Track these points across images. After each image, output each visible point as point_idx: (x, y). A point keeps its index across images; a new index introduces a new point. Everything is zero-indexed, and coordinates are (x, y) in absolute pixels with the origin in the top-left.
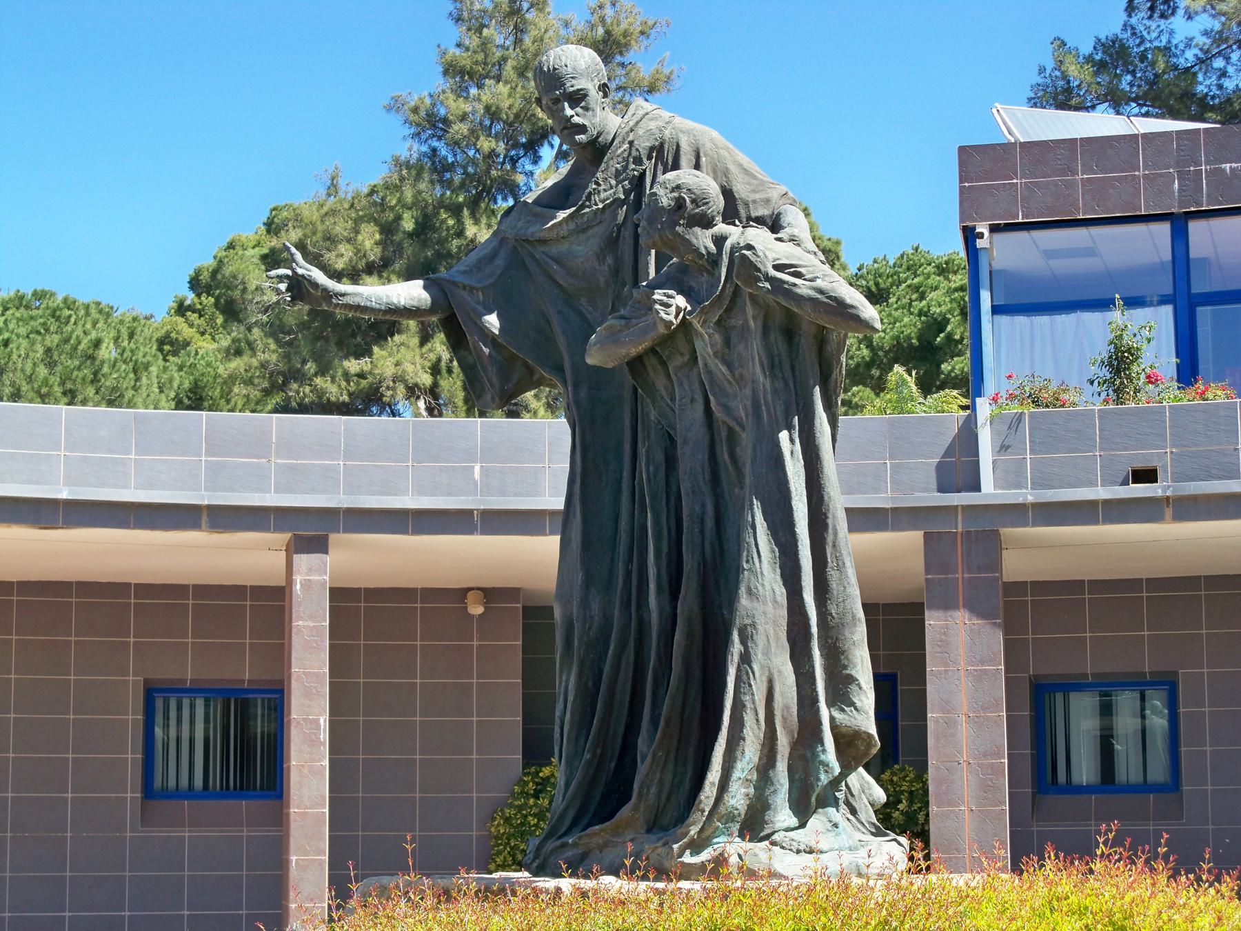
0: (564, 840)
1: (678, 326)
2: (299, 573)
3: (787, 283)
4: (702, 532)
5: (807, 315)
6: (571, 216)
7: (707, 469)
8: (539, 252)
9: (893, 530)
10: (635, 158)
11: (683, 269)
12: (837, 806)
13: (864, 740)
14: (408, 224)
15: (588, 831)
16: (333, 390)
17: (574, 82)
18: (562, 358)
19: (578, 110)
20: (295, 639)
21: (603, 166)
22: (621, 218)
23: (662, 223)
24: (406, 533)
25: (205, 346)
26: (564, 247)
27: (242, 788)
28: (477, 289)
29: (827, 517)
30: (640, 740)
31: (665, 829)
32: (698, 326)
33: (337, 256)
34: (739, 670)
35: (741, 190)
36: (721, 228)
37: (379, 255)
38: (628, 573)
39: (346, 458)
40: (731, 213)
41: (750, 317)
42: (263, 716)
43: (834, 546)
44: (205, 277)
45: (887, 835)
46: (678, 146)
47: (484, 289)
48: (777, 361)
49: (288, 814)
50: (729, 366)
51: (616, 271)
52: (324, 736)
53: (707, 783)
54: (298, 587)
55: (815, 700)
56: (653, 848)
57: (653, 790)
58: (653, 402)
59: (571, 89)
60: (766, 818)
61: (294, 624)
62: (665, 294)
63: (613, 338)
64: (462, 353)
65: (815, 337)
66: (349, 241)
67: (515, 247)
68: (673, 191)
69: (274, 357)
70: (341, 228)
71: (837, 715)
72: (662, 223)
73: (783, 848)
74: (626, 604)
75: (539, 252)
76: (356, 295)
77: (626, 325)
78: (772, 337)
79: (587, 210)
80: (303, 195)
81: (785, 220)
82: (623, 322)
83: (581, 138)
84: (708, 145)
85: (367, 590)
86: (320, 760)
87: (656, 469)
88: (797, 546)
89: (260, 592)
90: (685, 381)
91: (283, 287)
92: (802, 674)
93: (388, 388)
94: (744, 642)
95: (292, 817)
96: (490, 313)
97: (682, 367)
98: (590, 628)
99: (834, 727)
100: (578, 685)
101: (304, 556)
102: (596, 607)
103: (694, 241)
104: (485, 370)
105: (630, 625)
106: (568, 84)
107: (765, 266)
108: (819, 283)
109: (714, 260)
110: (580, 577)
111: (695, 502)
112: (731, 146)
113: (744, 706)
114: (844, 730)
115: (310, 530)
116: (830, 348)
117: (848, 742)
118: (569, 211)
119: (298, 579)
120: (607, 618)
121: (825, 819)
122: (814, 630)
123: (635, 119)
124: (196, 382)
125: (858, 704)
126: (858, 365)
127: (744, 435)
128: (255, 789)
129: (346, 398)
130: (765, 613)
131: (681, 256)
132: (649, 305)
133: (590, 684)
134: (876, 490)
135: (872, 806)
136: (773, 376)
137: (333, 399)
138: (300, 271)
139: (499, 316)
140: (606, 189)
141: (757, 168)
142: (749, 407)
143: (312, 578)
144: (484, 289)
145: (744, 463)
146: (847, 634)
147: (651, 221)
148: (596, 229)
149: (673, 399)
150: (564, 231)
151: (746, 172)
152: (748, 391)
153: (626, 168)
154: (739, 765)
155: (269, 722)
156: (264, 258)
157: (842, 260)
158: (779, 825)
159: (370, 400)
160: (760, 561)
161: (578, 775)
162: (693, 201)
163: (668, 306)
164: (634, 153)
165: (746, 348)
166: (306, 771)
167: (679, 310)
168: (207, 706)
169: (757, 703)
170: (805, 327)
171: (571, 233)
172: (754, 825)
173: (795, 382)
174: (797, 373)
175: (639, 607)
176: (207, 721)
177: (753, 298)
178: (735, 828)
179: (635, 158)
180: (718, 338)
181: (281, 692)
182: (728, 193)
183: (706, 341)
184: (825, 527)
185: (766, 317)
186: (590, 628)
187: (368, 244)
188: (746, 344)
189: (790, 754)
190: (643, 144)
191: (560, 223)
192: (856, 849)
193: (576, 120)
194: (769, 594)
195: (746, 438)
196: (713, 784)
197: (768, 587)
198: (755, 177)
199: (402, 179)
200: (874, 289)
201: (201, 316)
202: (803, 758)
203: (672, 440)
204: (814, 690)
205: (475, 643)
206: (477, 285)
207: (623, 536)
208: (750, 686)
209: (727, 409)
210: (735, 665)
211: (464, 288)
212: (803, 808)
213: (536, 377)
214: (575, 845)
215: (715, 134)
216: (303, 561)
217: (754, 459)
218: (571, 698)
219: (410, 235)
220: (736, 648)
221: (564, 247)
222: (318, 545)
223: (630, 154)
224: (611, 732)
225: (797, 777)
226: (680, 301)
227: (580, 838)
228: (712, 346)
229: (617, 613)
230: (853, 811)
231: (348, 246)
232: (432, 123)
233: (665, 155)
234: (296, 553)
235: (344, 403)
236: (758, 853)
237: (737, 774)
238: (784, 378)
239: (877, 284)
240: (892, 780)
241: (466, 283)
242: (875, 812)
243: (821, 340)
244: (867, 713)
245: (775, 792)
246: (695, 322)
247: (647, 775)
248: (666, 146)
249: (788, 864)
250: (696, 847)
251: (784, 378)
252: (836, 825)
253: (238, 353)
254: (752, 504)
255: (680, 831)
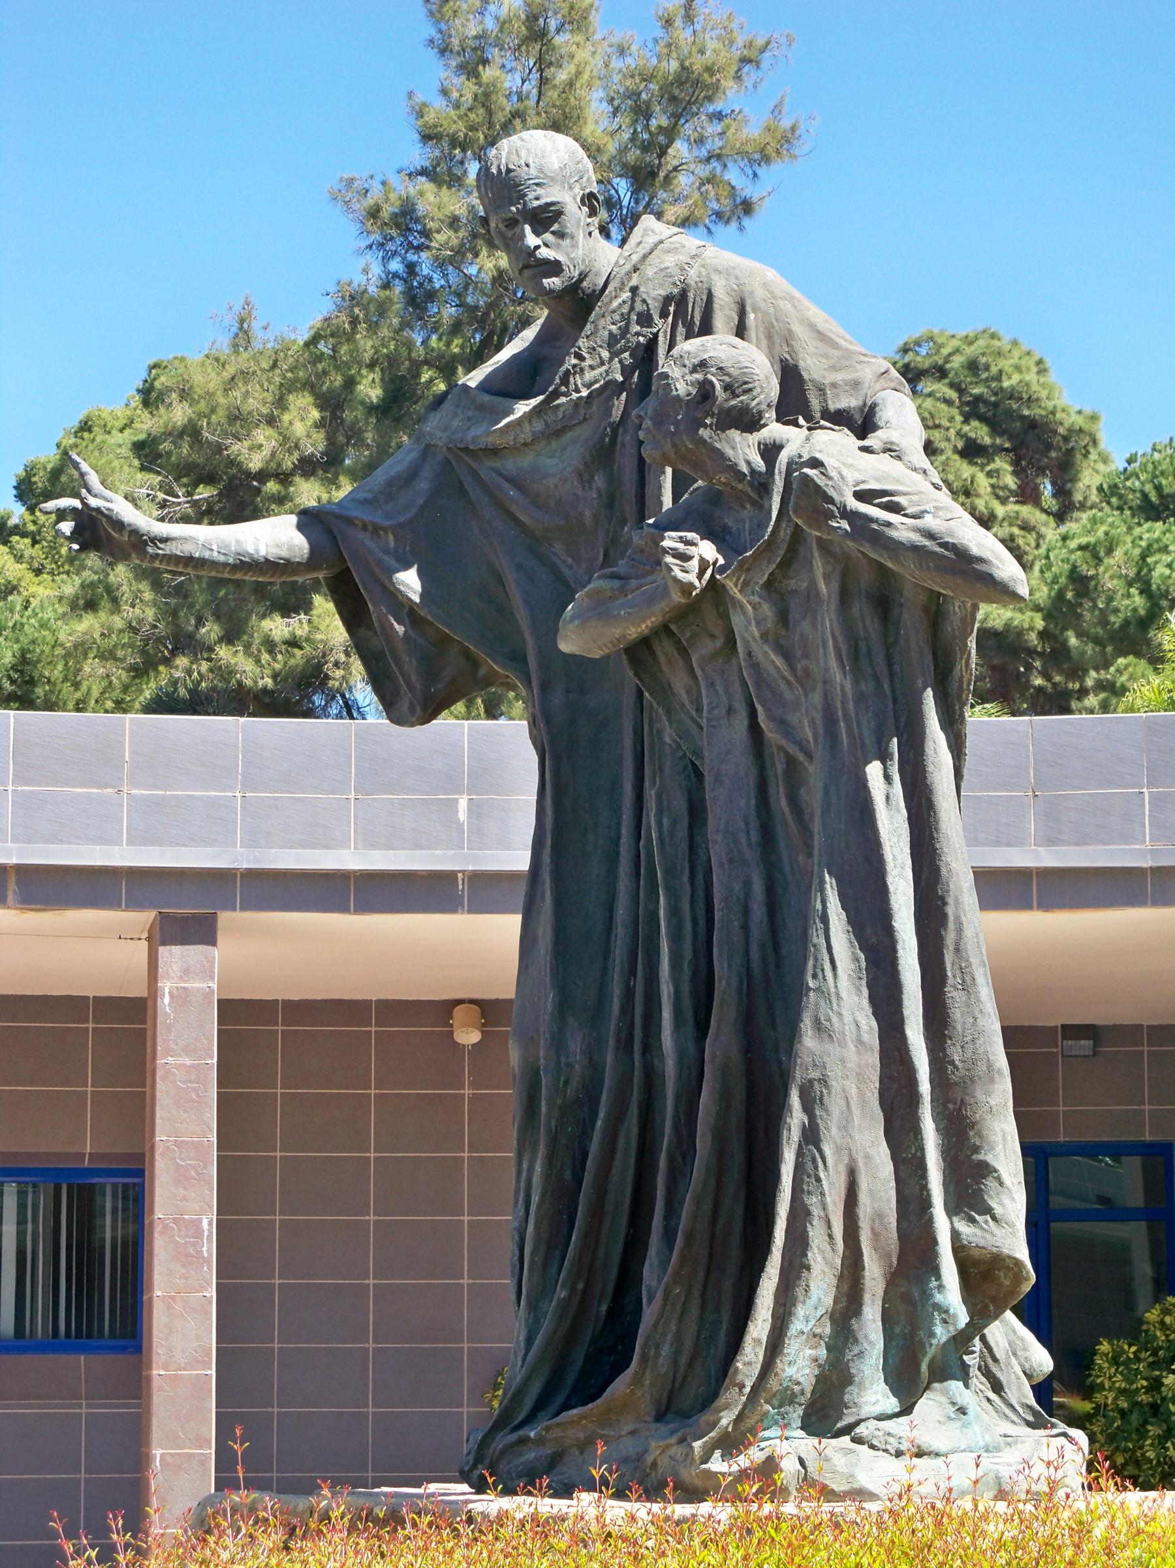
0: (521, 1432)
1: (703, 590)
2: (168, 977)
3: (876, 521)
4: (745, 927)
5: (908, 572)
6: (537, 411)
7: (754, 824)
8: (486, 468)
9: (1155, 903)
10: (639, 315)
11: (714, 498)
12: (965, 1378)
13: (1009, 1269)
14: (370, 389)
15: (559, 1419)
16: (250, 670)
17: (540, 191)
18: (524, 641)
19: (548, 236)
20: (161, 1087)
21: (588, 328)
22: (617, 413)
23: (677, 423)
24: (344, 909)
25: (41, 591)
26: (526, 461)
27: (79, 1335)
28: (385, 530)
29: (945, 904)
30: (646, 1270)
31: (686, 1415)
32: (735, 591)
33: (251, 449)
34: (800, 1154)
35: (812, 366)
36: (774, 430)
37: (321, 447)
38: (629, 994)
39: (245, 787)
40: (795, 400)
41: (820, 577)
42: (114, 1211)
43: (957, 950)
44: (40, 480)
45: (1053, 1426)
46: (710, 295)
47: (397, 529)
48: (863, 647)
49: (149, 1379)
50: (786, 654)
51: (610, 500)
52: (209, 1248)
53: (748, 1340)
54: (167, 1000)
55: (927, 1204)
56: (660, 1448)
57: (666, 1350)
58: (669, 712)
59: (536, 203)
60: (847, 1398)
61: (160, 1062)
62: (681, 540)
63: (601, 608)
64: (362, 632)
65: (926, 609)
66: (271, 421)
67: (447, 461)
68: (694, 370)
69: (150, 614)
70: (256, 401)
71: (963, 1227)
72: (677, 423)
73: (872, 1447)
74: (625, 1045)
75: (486, 468)
76: (186, 539)
77: (622, 587)
78: (855, 610)
79: (563, 400)
80: (194, 342)
81: (885, 414)
82: (616, 584)
83: (553, 282)
84: (760, 293)
85: (286, 1003)
86: (202, 1288)
87: (674, 823)
88: (895, 951)
89: (109, 1007)
90: (718, 680)
91: (67, 527)
92: (905, 1160)
93: (337, 664)
94: (808, 1108)
95: (156, 1383)
96: (406, 566)
97: (714, 655)
98: (567, 1082)
99: (959, 1249)
100: (546, 1177)
101: (176, 949)
102: (576, 1046)
103: (729, 452)
104: (398, 664)
105: (631, 1079)
106: (531, 196)
107: (841, 494)
108: (929, 522)
109: (762, 484)
110: (548, 1000)
111: (732, 877)
112: (797, 294)
113: (808, 1214)
114: (976, 1253)
115: (187, 906)
116: (951, 626)
117: (982, 1275)
118: (541, 398)
119: (166, 986)
120: (594, 1066)
121: (944, 1400)
122: (925, 1087)
123: (642, 251)
124: (23, 652)
125: (998, 1210)
126: (1126, 623)
127: (811, 769)
128: (101, 1334)
129: (269, 682)
130: (843, 1061)
131: (708, 478)
132: (654, 559)
133: (568, 1174)
134: (1127, 838)
135: (1029, 1377)
136: (857, 674)
137: (248, 682)
138: (93, 502)
139: (421, 574)
140: (593, 366)
141: (841, 331)
142: (819, 722)
143: (190, 987)
144: (397, 529)
145: (812, 816)
146: (979, 1094)
147: (660, 420)
148: (578, 431)
149: (699, 710)
150: (526, 434)
151: (822, 336)
152: (817, 698)
153: (625, 331)
154: (800, 1311)
155: (125, 1220)
156: (139, 447)
157: (1102, 445)
158: (866, 1411)
159: (309, 685)
160: (835, 975)
161: (547, 1323)
162: (727, 387)
163: (685, 558)
164: (639, 307)
165: (815, 626)
166: (178, 1307)
167: (704, 565)
168: (22, 1195)
169: (830, 1207)
170: (908, 592)
171: (537, 438)
172: (825, 1412)
173: (892, 681)
174: (897, 667)
175: (646, 1048)
176: (21, 1221)
177: (823, 546)
178: (796, 1414)
179: (639, 315)
180: (767, 610)
181: (140, 1173)
182: (790, 375)
183: (750, 615)
184: (942, 919)
185: (844, 575)
186: (567, 1082)
187: (299, 429)
188: (815, 618)
189: (886, 1292)
190: (654, 293)
191: (519, 421)
192: (997, 1449)
193: (544, 253)
194: (849, 1029)
195: (815, 773)
196: (757, 1341)
197: (848, 1018)
198: (835, 345)
199: (354, 321)
200: (1153, 497)
201: (35, 542)
202: (907, 1298)
203: (699, 775)
204: (924, 1187)
205: (467, 1092)
206: (386, 523)
207: (621, 932)
208: (818, 1180)
209: (783, 725)
210: (794, 1146)
211: (364, 527)
212: (908, 1383)
213: (482, 672)
214: (540, 1441)
215: (771, 274)
216: (173, 957)
217: (826, 807)
218: (535, 1198)
219: (371, 409)
220: (796, 1117)
221: (526, 461)
222: (201, 931)
223: (632, 308)
224: (601, 1253)
225: (898, 1330)
226: (707, 550)
227: (548, 1429)
228: (758, 623)
229: (610, 1057)
230: (997, 1387)
231: (269, 431)
232: (401, 225)
233: (690, 311)
234: (163, 943)
235: (265, 690)
236: (838, 1458)
237: (797, 1325)
238: (875, 677)
239: (1158, 488)
240: (1162, 1322)
241: (367, 518)
242: (1033, 1387)
243: (935, 612)
244: (1012, 1225)
245: (861, 1354)
246: (730, 584)
247: (656, 1325)
248: (691, 295)
249: (876, 1472)
250: (731, 1444)
251: (875, 677)
252: (962, 1411)
253: (91, 605)
254: (822, 882)
255: (706, 1418)
